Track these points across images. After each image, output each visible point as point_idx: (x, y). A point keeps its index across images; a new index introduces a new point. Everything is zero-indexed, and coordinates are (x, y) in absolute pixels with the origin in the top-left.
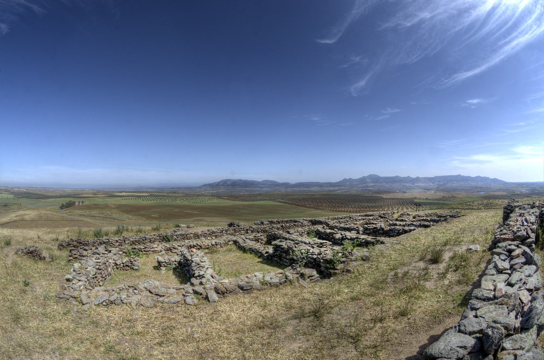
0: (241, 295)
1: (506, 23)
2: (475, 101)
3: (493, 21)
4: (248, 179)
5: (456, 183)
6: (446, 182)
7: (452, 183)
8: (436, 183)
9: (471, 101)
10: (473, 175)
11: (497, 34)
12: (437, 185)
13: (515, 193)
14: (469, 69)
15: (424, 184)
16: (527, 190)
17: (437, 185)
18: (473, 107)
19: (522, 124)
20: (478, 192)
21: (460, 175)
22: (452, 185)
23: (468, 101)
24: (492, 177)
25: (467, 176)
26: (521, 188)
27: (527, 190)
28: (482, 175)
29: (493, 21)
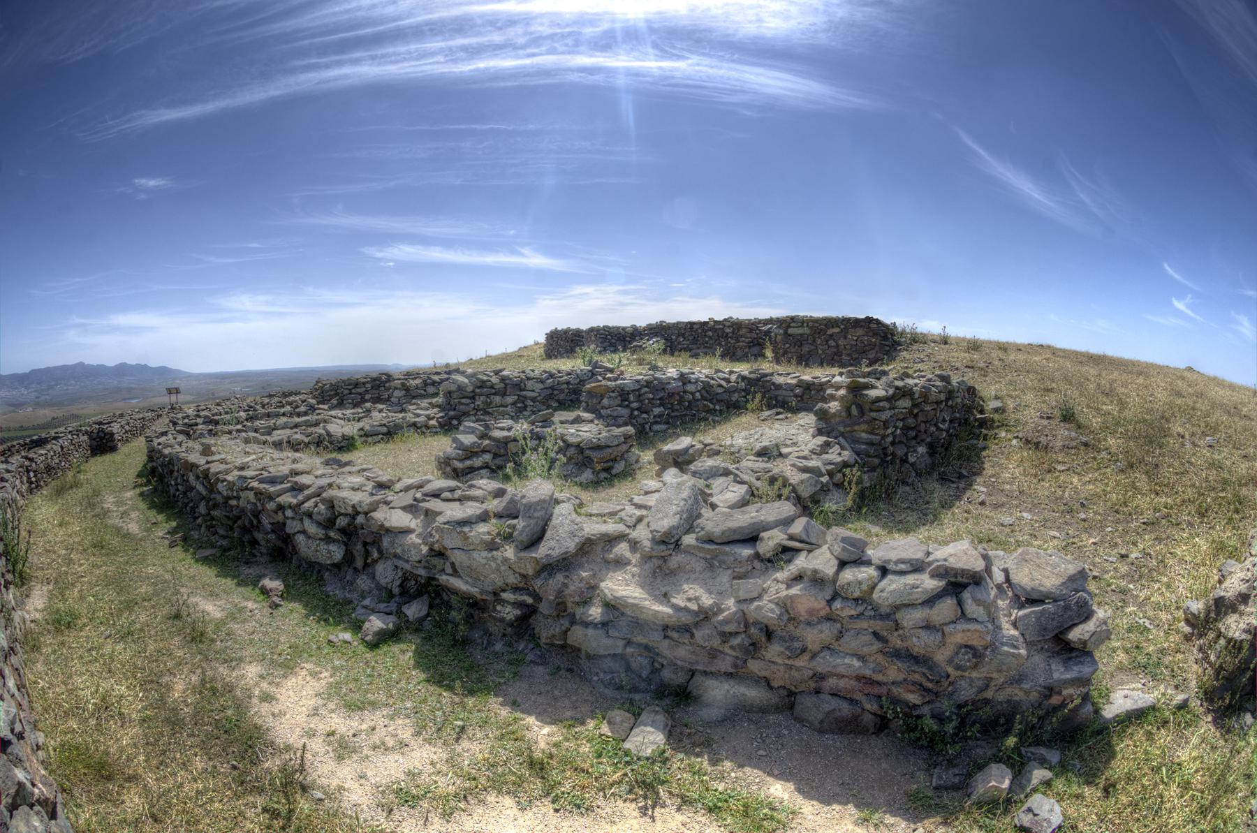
0: (471, 650)
1: (381, 20)
2: (152, 183)
3: (337, 9)
4: (174, 365)
5: (73, 382)
6: (53, 383)
7: (65, 384)
8: (33, 386)
9: (143, 181)
10: (111, 362)
11: (306, 42)
12: (35, 391)
13: (216, 395)
14: (172, 105)
15: (9, 391)
16: (247, 387)
17: (35, 391)
18: (143, 196)
19: (255, 245)
20: (125, 399)
21: (81, 364)
22: (65, 388)
23: (137, 181)
24: (153, 364)
25: (137, 365)
26: (231, 383)
27: (247, 387)
28: (36, 368)
29: (337, 9)
